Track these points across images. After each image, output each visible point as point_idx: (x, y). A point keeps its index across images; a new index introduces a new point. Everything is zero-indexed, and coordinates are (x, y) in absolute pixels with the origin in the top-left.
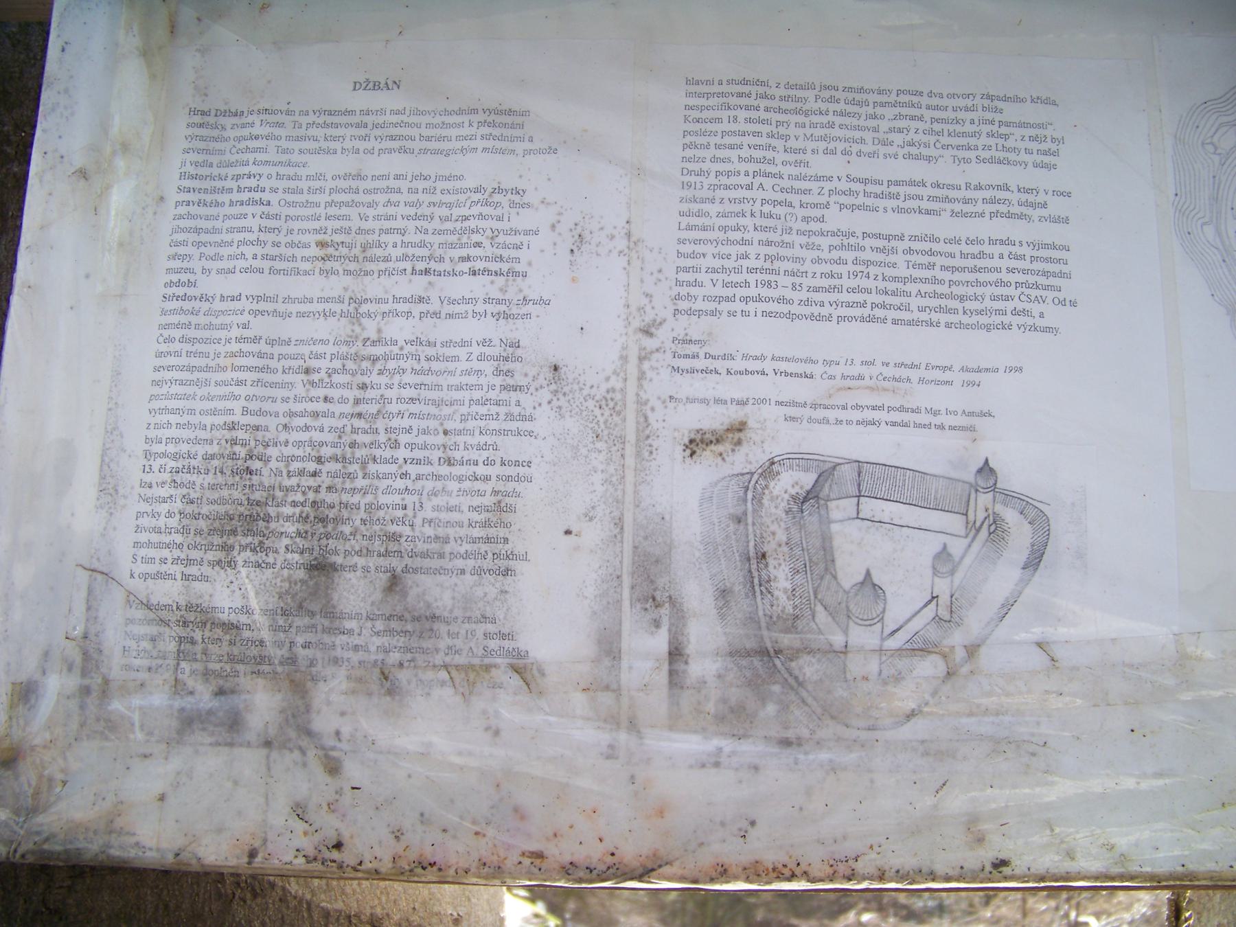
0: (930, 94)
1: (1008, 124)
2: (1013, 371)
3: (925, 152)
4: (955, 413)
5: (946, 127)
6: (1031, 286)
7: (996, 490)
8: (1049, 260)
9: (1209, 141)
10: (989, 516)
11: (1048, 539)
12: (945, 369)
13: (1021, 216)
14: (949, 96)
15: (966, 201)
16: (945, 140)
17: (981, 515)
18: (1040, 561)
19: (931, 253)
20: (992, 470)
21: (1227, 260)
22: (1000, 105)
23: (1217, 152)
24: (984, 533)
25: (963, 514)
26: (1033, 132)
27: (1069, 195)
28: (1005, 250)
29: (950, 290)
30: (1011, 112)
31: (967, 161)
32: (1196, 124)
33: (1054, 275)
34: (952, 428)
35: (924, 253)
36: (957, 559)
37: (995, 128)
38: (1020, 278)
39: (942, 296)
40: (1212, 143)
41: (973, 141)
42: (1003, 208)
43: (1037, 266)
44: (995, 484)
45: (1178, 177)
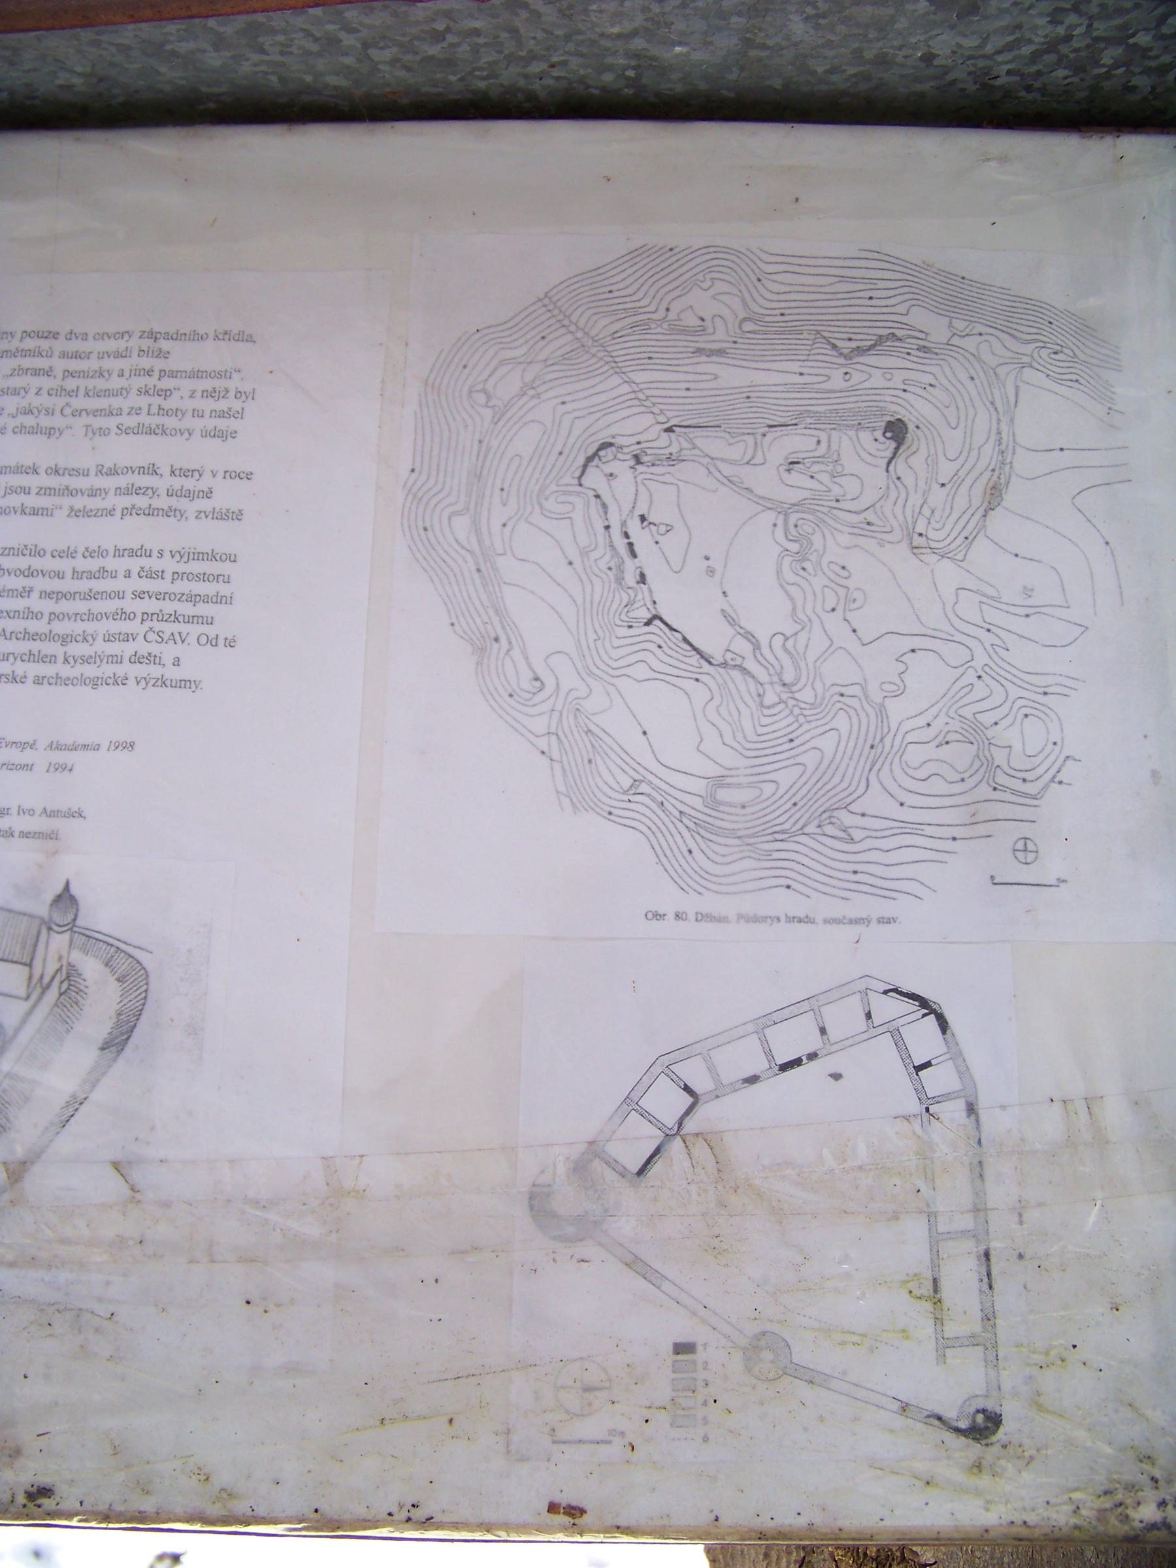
0: (71, 335)
1: (173, 374)
2: (120, 748)
3: (45, 421)
4: (31, 812)
5: (82, 383)
6: (166, 617)
7: (75, 929)
8: (203, 577)
9: (479, 387)
10: (61, 966)
11: (144, 1005)
12: (24, 746)
13: (169, 512)
14: (97, 336)
15: (93, 493)
16: (79, 403)
17: (52, 967)
18: (128, 1038)
19: (30, 573)
20: (73, 900)
21: (483, 568)
22: (165, 345)
23: (489, 404)
24: (52, 994)
25: (24, 964)
26: (208, 384)
27: (249, 476)
28: (135, 564)
29: (49, 627)
30: (182, 356)
31: (104, 432)
32: (463, 363)
33: (206, 599)
34: (25, 835)
35: (18, 573)
36: (10, 1032)
37: (151, 381)
38: (152, 606)
39: (34, 637)
40: (484, 391)
41: (116, 402)
42: (142, 502)
43: (183, 586)
44: (75, 920)
45: (420, 442)
